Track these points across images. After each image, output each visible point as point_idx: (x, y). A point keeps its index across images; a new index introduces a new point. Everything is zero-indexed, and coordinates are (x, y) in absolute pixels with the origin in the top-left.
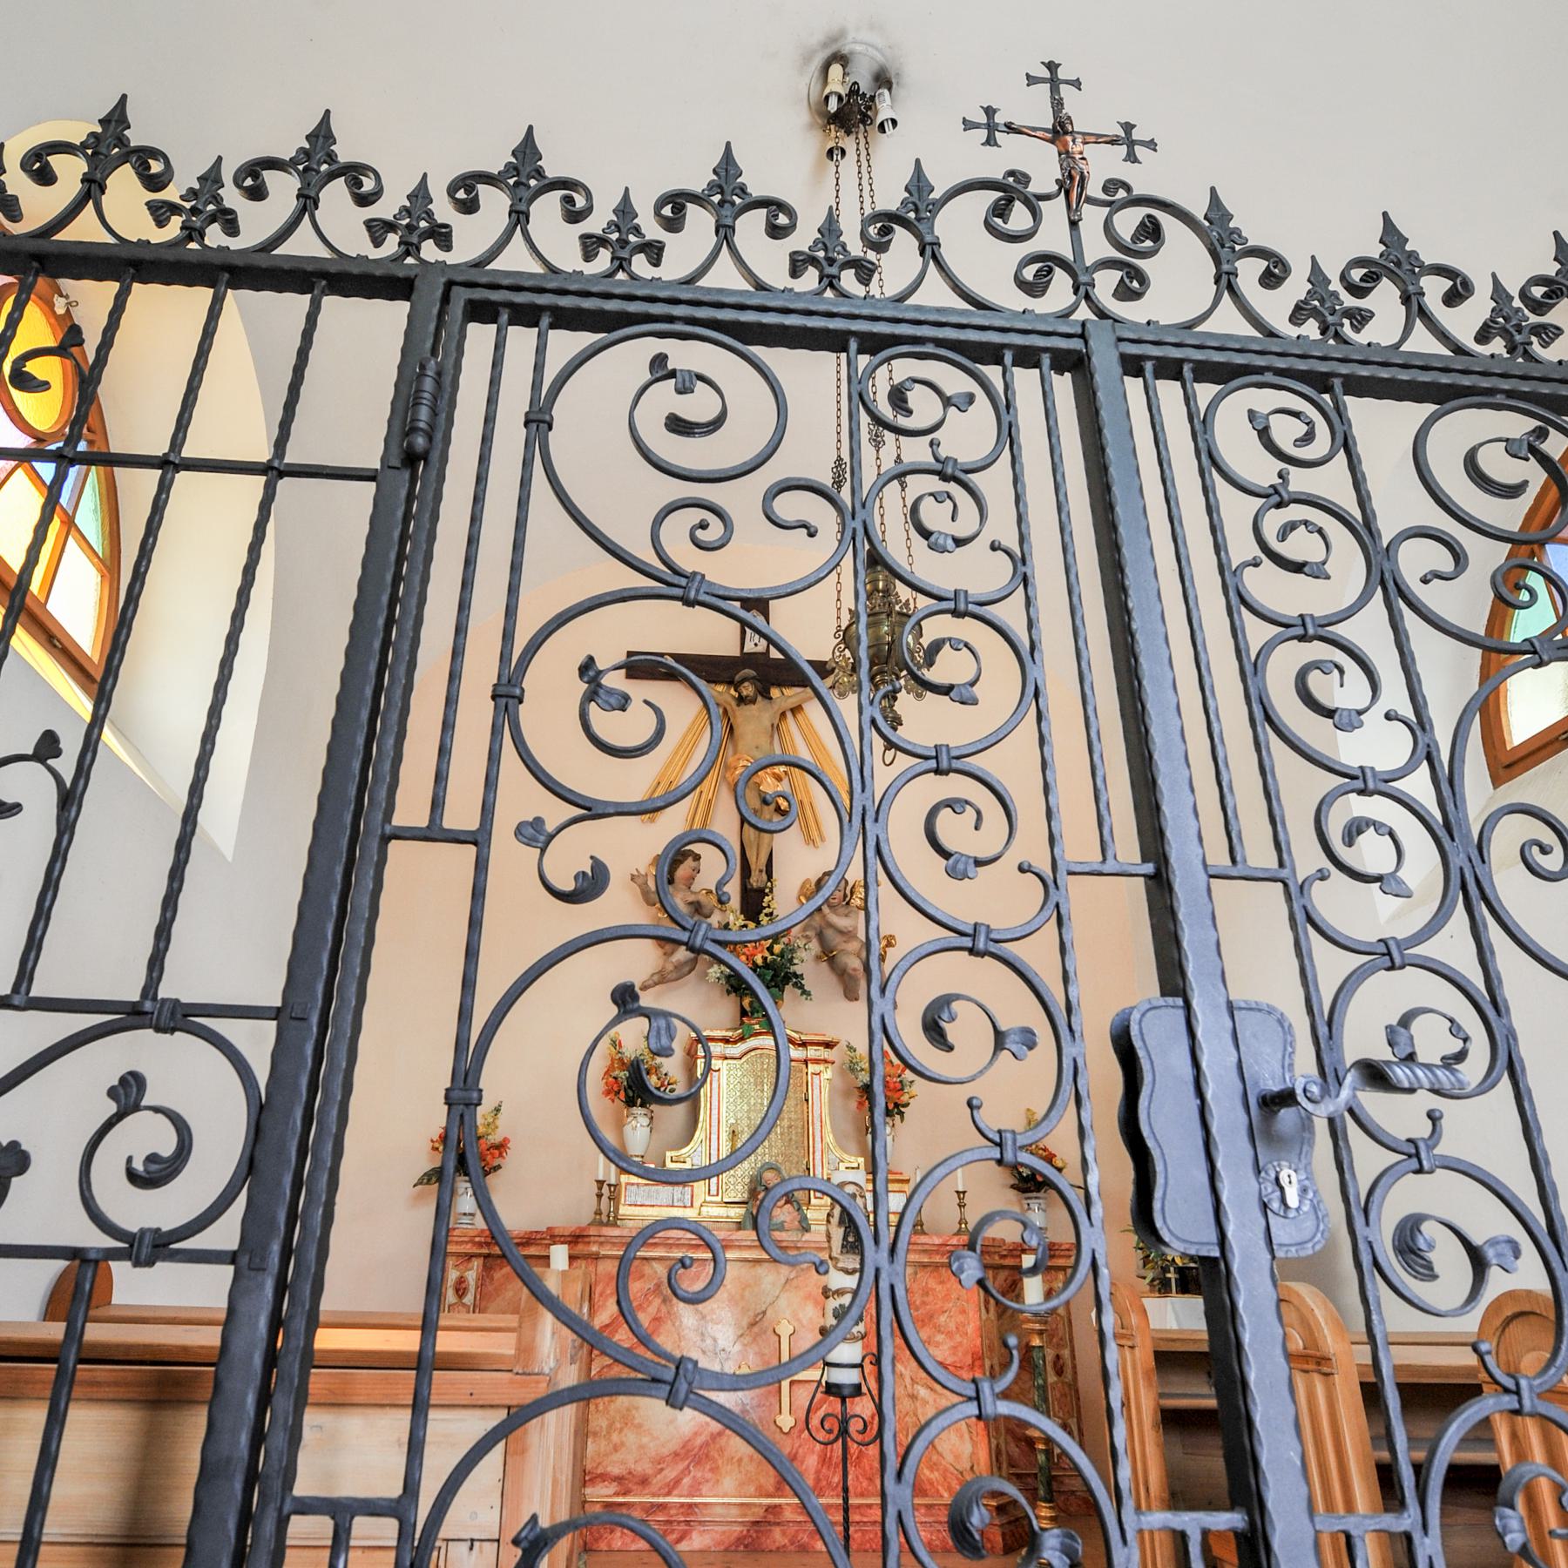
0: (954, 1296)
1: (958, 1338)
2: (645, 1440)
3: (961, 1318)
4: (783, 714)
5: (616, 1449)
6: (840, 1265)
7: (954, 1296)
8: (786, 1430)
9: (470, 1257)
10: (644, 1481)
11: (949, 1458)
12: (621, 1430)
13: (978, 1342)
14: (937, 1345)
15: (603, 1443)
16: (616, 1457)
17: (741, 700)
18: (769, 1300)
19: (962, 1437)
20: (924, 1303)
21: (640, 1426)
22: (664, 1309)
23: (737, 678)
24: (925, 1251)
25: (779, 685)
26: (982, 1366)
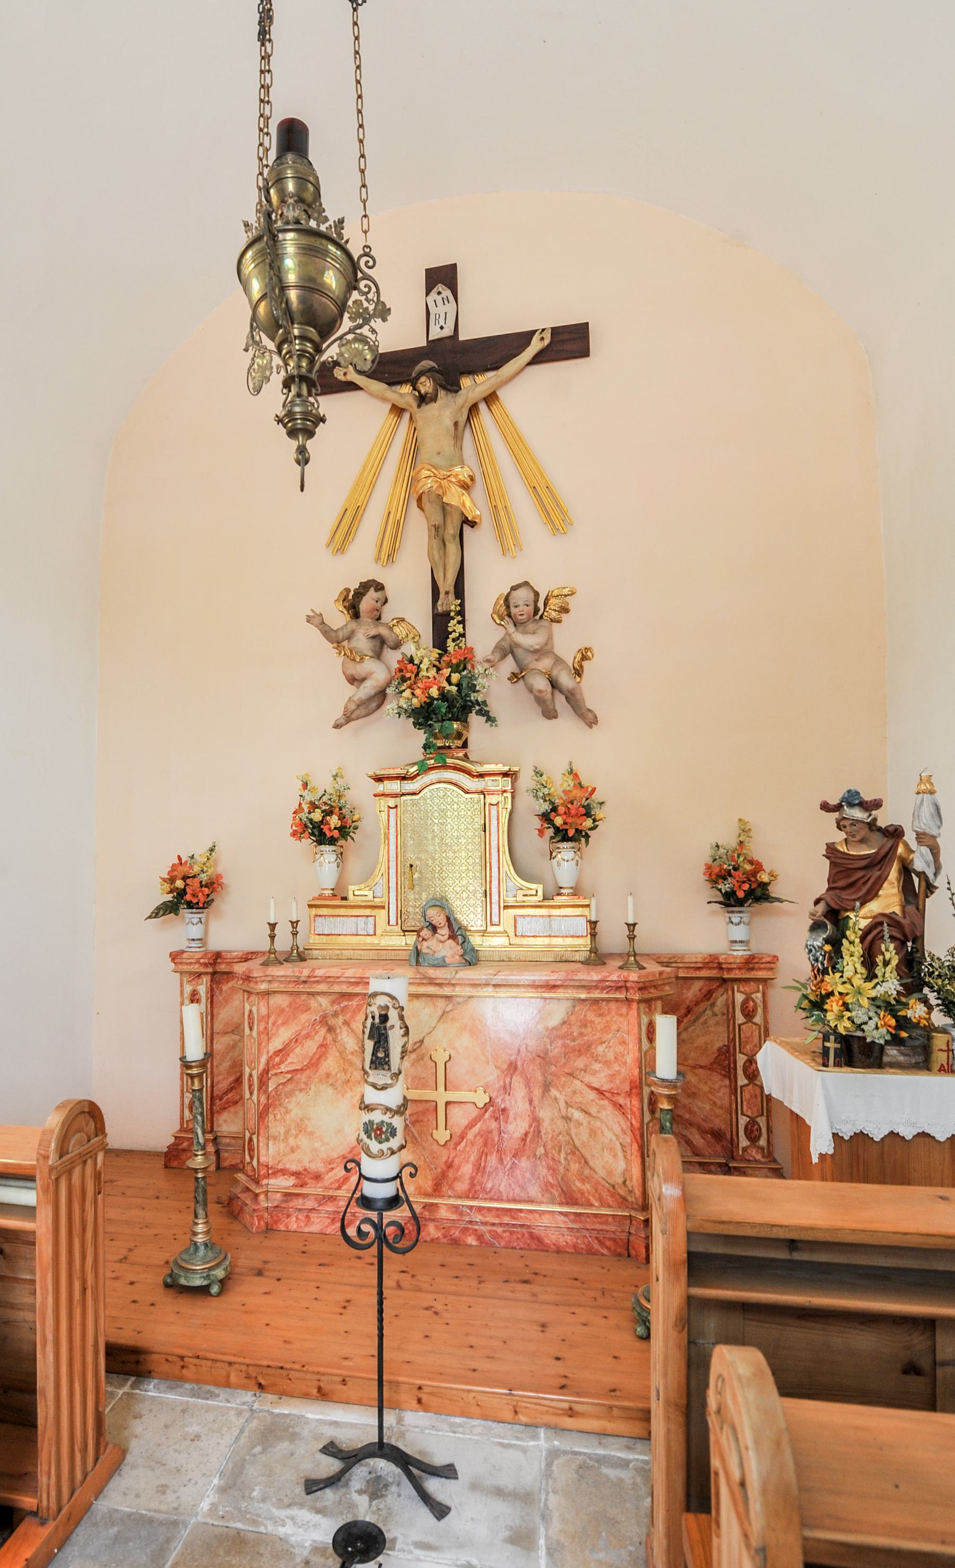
0: (614, 1027)
1: (616, 1067)
2: (317, 1145)
3: (620, 1049)
4: (474, 409)
5: (293, 1150)
6: (370, 1080)
7: (614, 1027)
8: (442, 1143)
9: (199, 975)
10: (318, 1177)
11: (602, 1173)
12: (296, 1136)
13: (636, 1072)
14: (594, 1073)
15: (282, 1145)
16: (292, 1156)
17: (423, 400)
18: (426, 1030)
19: (615, 1156)
20: (581, 1034)
21: (312, 1133)
22: (329, 1037)
23: (414, 375)
24: (583, 987)
25: (472, 372)
26: (640, 1094)
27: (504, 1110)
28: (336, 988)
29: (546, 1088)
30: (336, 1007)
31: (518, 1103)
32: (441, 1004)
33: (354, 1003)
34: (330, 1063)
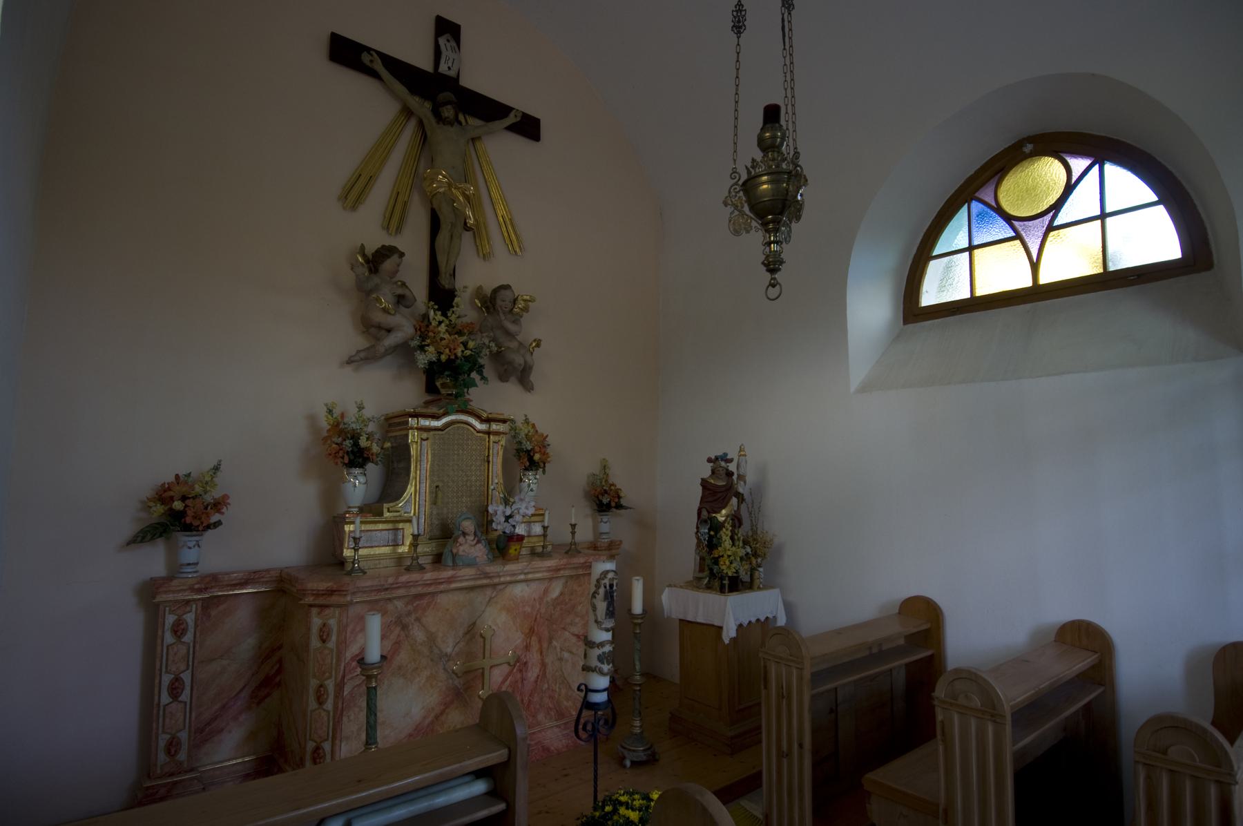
27: (526, 663)
28: (414, 591)
29: (550, 640)
30: (410, 607)
31: (534, 657)
32: (489, 592)
33: (425, 601)
34: (403, 657)
